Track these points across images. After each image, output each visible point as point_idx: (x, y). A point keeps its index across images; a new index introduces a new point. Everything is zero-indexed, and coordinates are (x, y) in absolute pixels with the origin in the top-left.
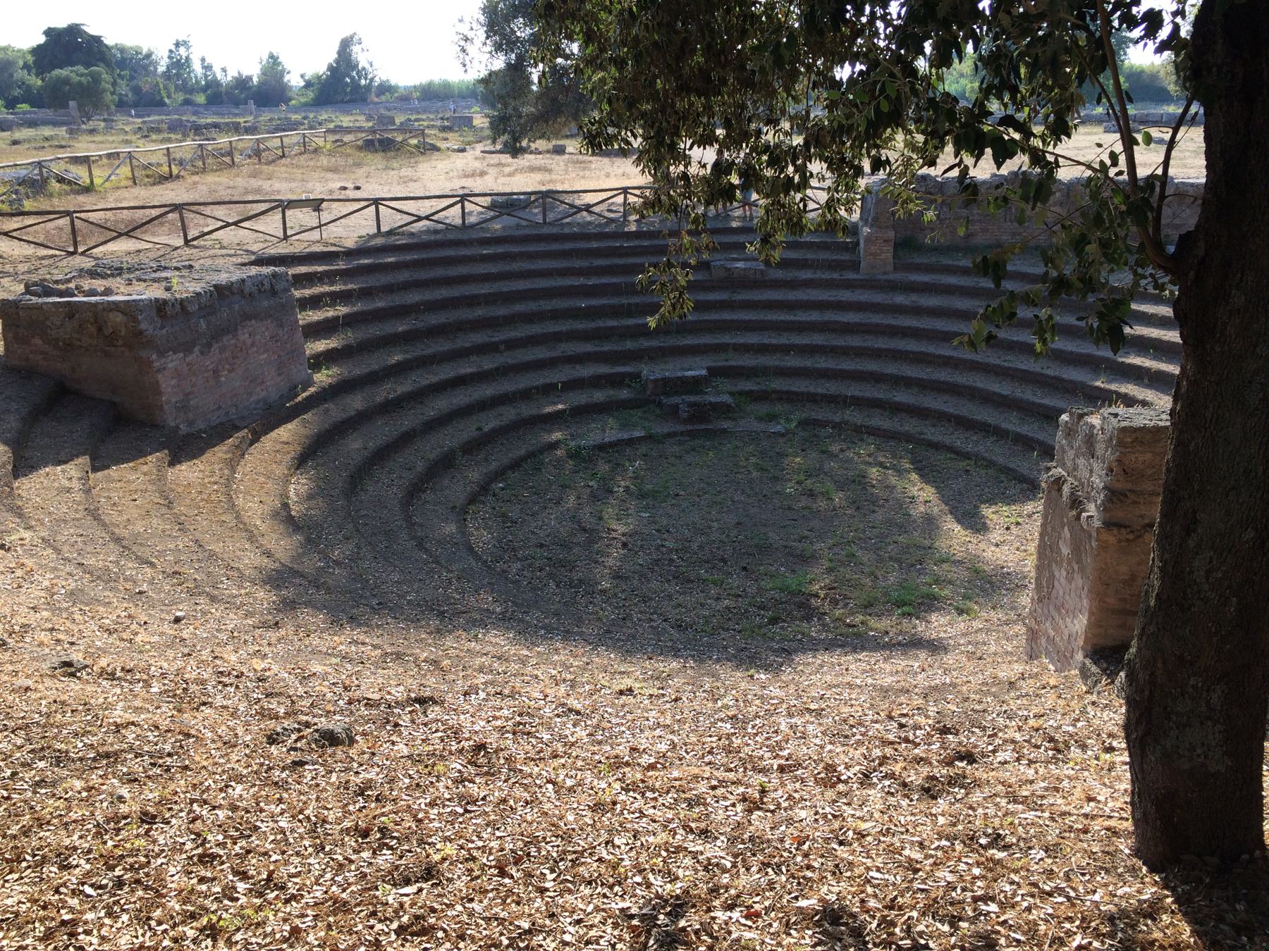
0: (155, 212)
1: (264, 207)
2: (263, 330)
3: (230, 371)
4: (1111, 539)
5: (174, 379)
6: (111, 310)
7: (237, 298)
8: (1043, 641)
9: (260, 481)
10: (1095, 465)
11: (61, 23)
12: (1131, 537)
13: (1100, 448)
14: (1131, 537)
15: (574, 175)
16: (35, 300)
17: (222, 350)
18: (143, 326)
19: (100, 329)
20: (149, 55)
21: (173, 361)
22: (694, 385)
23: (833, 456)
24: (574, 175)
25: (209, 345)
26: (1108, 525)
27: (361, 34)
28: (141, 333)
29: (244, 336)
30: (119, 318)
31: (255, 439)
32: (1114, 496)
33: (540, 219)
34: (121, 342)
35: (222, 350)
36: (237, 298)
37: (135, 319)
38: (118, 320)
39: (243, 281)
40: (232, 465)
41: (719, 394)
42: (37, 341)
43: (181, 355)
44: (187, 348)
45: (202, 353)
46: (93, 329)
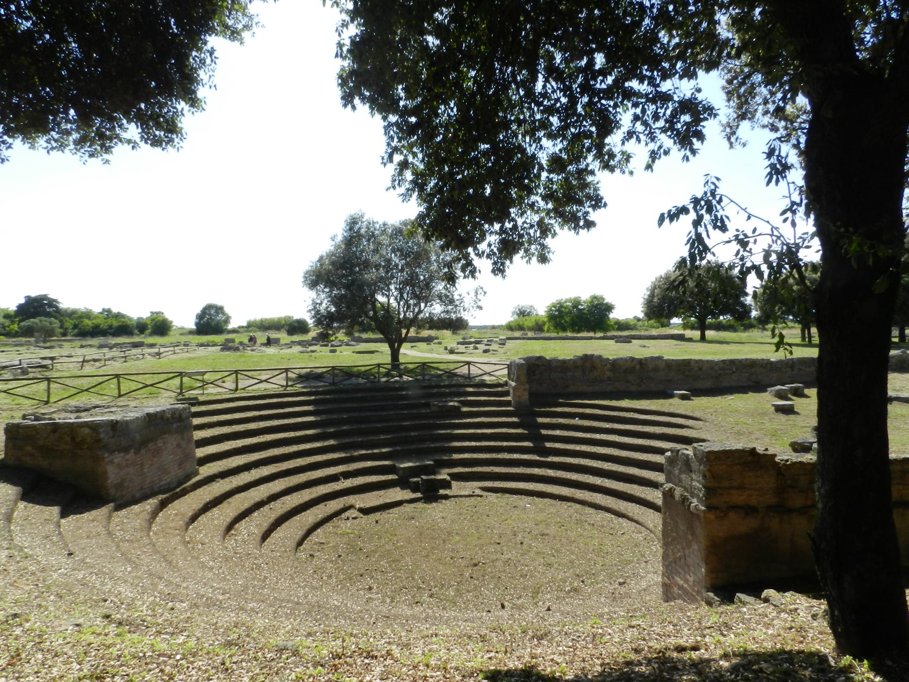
0: (100, 379)
1: (172, 375)
2: (171, 441)
4: (711, 516)
5: (115, 469)
8: (675, 589)
9: (508, 262)
10: (694, 476)
11: (34, 294)
12: (722, 515)
13: (695, 465)
14: (722, 515)
16: (30, 422)
18: (102, 436)
19: (73, 439)
21: (118, 458)
26: (710, 508)
27: (353, 211)
28: (100, 440)
31: (163, 505)
32: (710, 491)
34: (86, 446)
39: (164, 411)
40: (154, 514)
41: (443, 475)
42: (29, 448)
43: (122, 454)
44: (126, 450)
45: (135, 453)
46: (68, 439)
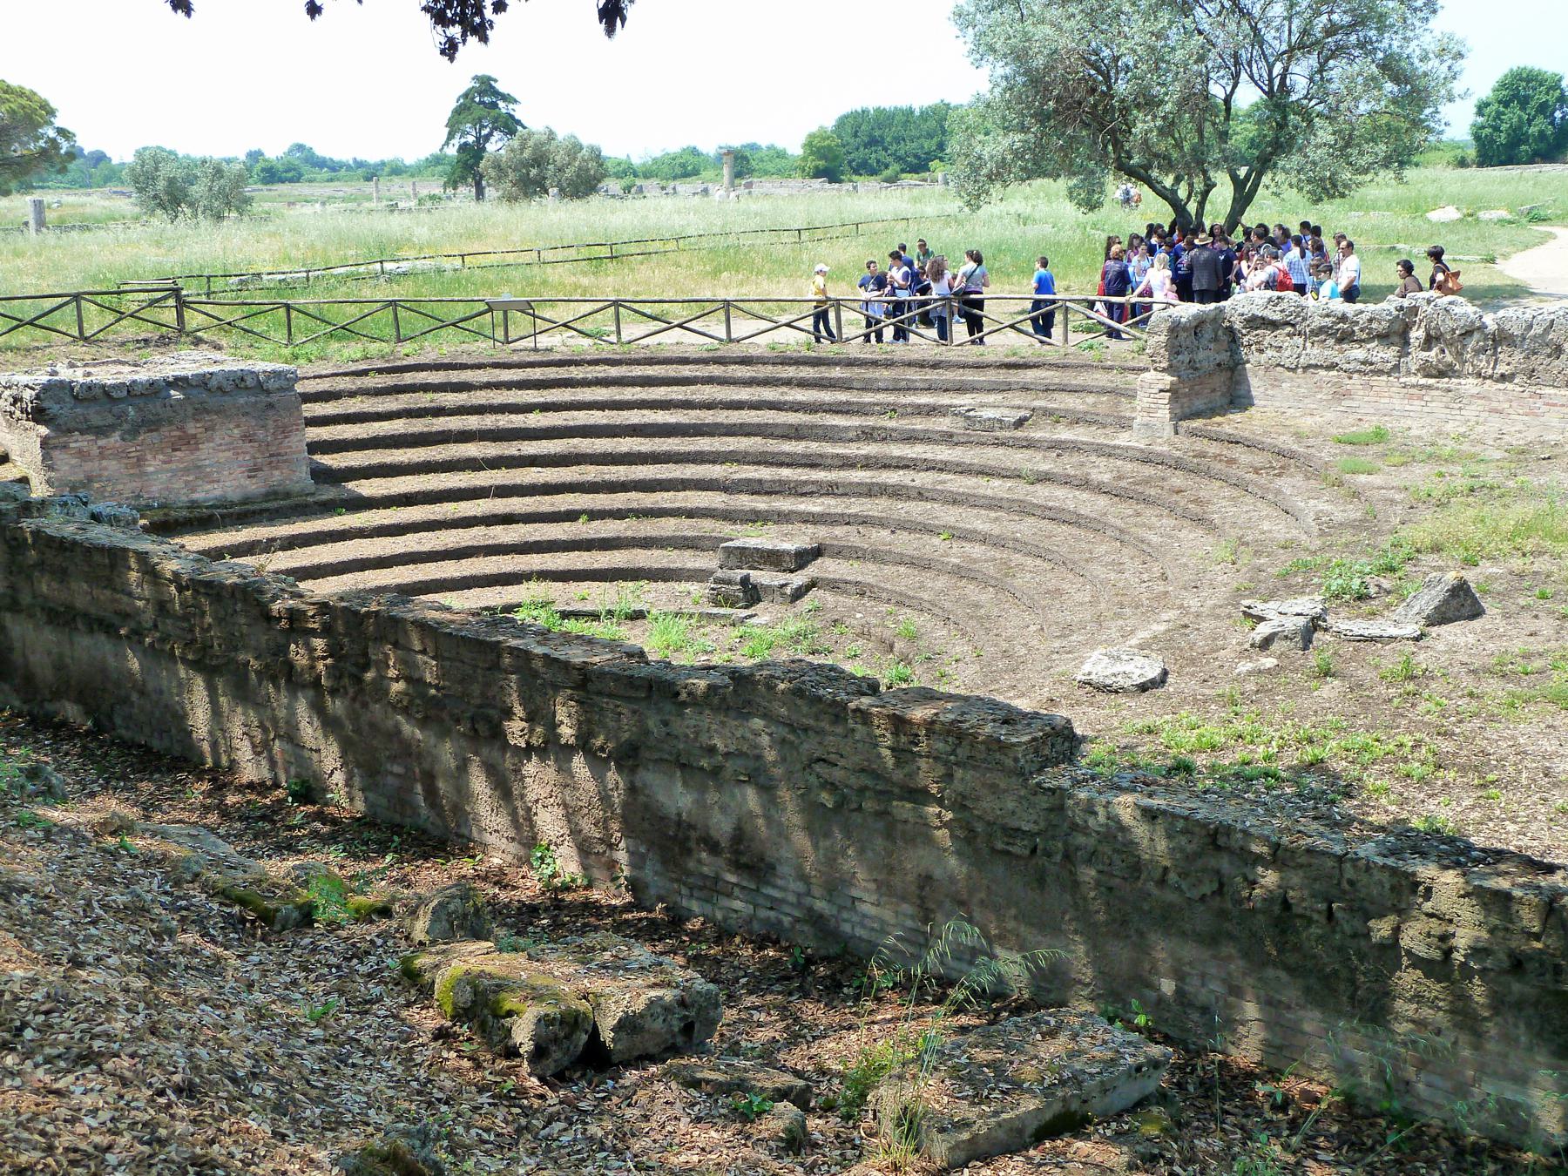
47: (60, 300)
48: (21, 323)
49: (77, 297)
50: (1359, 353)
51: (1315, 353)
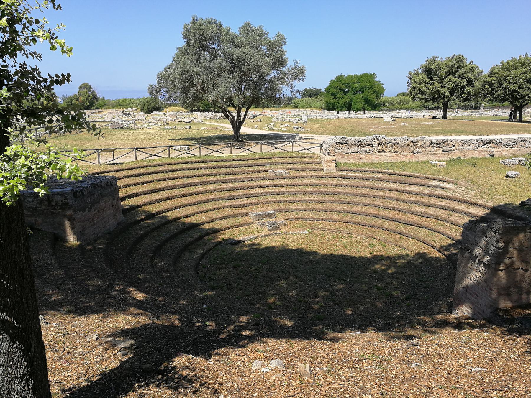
3: (98, 218)
6: (56, 195)
7: (100, 188)
15: (81, 99)
17: (95, 209)
20: (374, 74)
22: (271, 216)
23: (17, 155)
24: (81, 99)
25: (91, 208)
28: (68, 203)
29: (102, 204)
30: (59, 198)
33: (290, 150)
35: (95, 209)
36: (100, 188)
37: (66, 198)
38: (59, 199)
41: (280, 219)
45: (89, 211)
47: (92, 151)
48: (151, 155)
49: (136, 150)
50: (364, 149)
51: (353, 149)
